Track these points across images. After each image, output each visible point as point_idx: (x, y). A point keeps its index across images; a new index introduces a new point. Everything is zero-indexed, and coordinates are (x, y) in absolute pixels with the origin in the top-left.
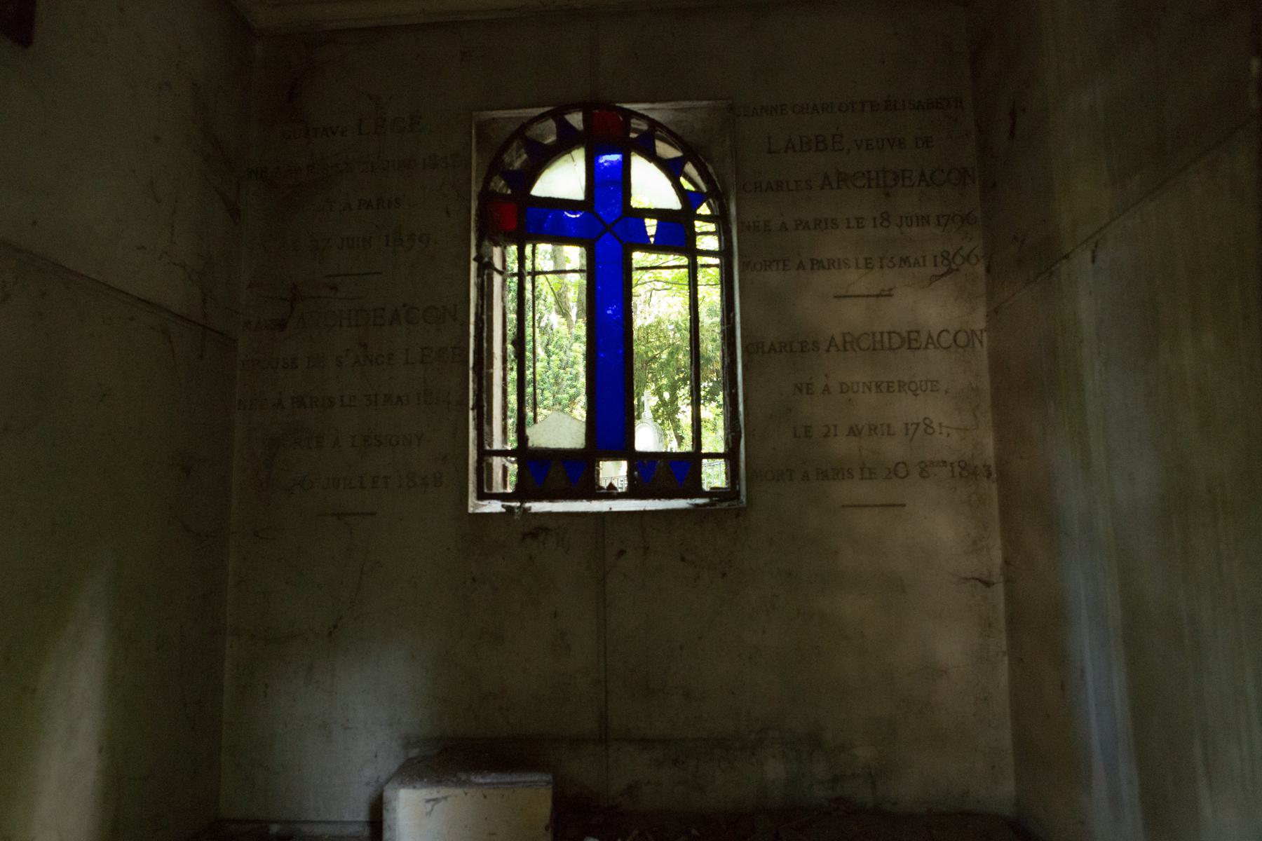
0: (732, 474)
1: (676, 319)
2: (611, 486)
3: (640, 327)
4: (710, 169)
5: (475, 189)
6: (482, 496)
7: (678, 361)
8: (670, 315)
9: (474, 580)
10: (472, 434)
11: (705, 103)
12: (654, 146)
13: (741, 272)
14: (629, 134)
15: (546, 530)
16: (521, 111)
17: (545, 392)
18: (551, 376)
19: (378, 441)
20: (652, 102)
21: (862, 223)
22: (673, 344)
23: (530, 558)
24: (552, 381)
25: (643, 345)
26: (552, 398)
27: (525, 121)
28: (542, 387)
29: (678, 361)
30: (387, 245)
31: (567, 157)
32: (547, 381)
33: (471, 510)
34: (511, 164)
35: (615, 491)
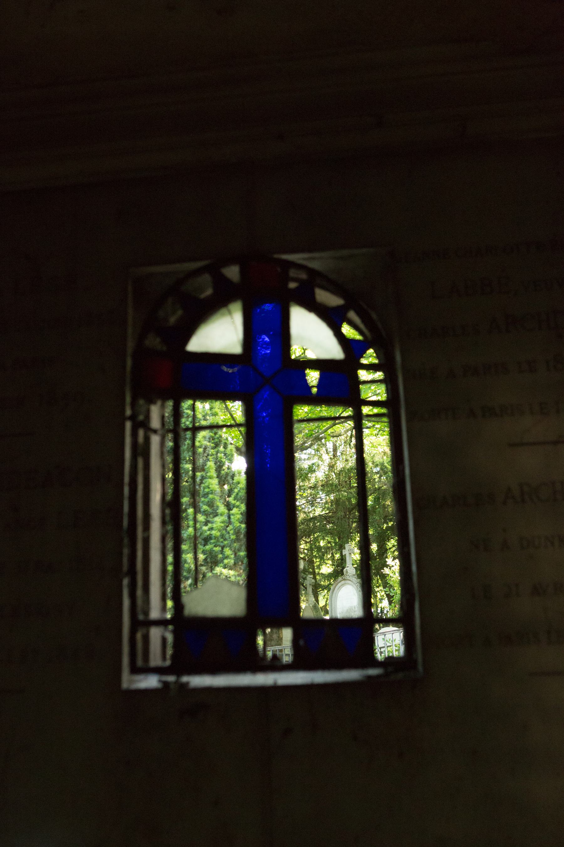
0: (409, 640)
1: (381, 460)
3: (341, 471)
4: (374, 316)
5: (131, 345)
6: (135, 670)
7: (385, 508)
8: (374, 456)
10: (126, 602)
11: (364, 250)
12: (313, 294)
13: (408, 421)
14: (287, 284)
17: (225, 550)
18: (232, 532)
20: (310, 251)
22: (379, 488)
24: (233, 537)
25: (345, 491)
26: (233, 556)
28: (222, 544)
29: (385, 508)
31: (224, 310)
32: (227, 536)
33: (125, 685)
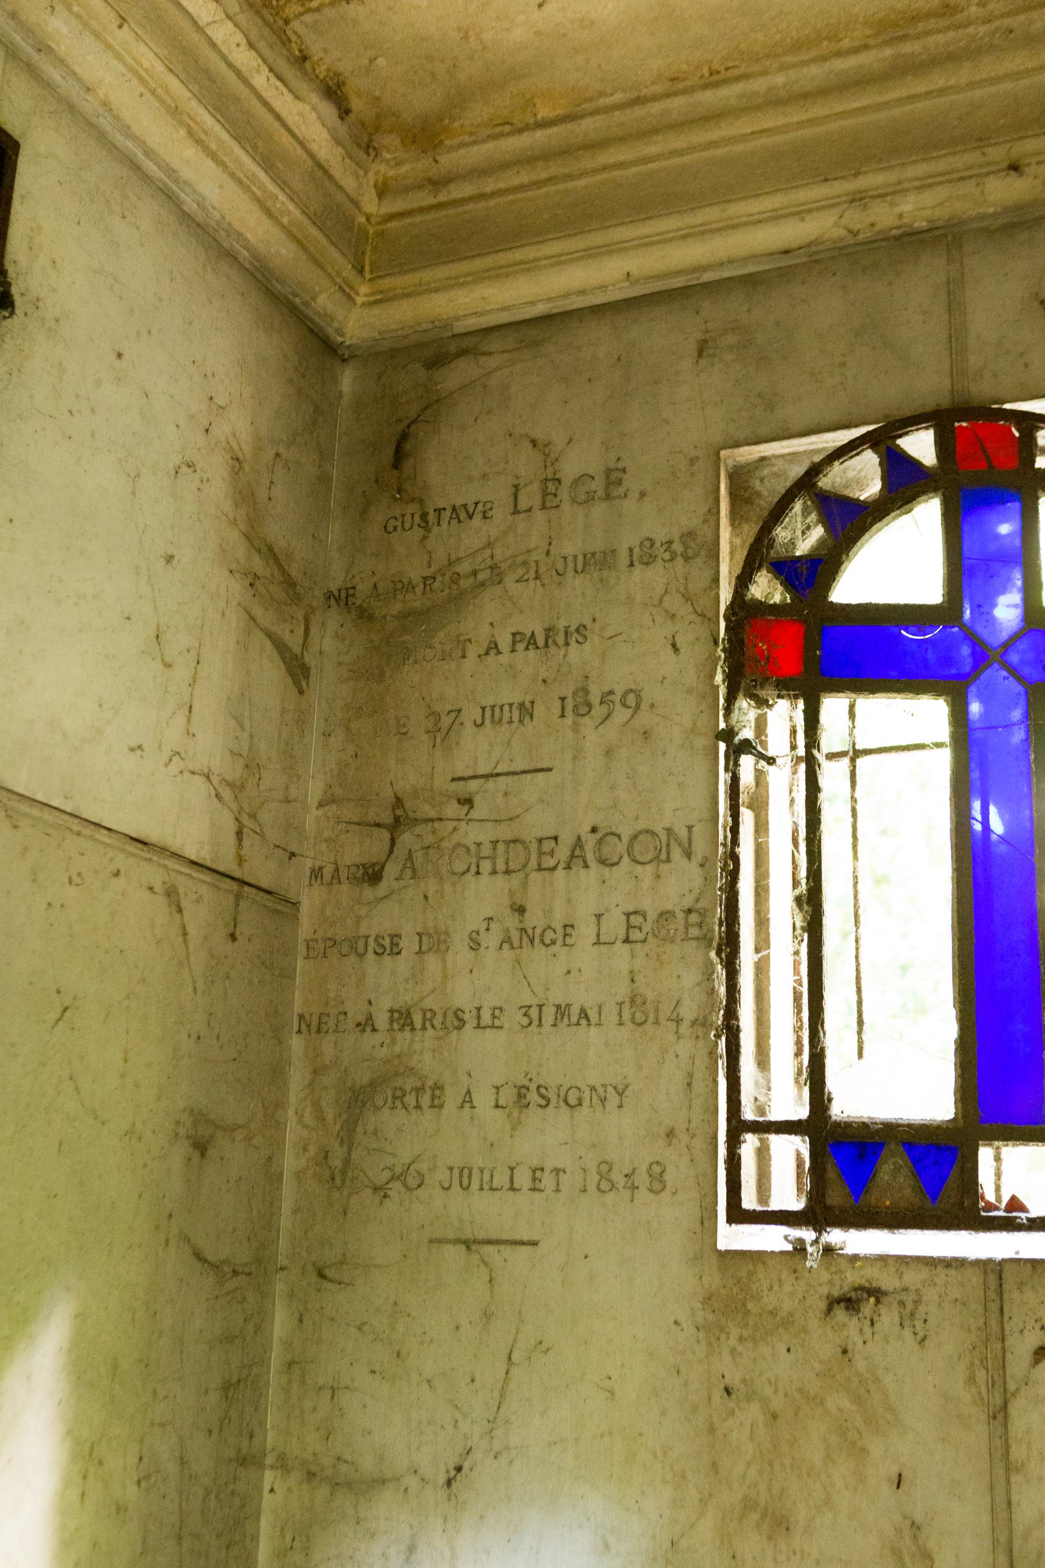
2: (1015, 1204)
6: (737, 1215)
9: (728, 1391)
15: (876, 1293)
16: (813, 438)
19: (543, 1097)
21: (552, 853)
23: (845, 1352)
27: (817, 459)
30: (563, 716)
34: (792, 543)
35: (1023, 1215)
